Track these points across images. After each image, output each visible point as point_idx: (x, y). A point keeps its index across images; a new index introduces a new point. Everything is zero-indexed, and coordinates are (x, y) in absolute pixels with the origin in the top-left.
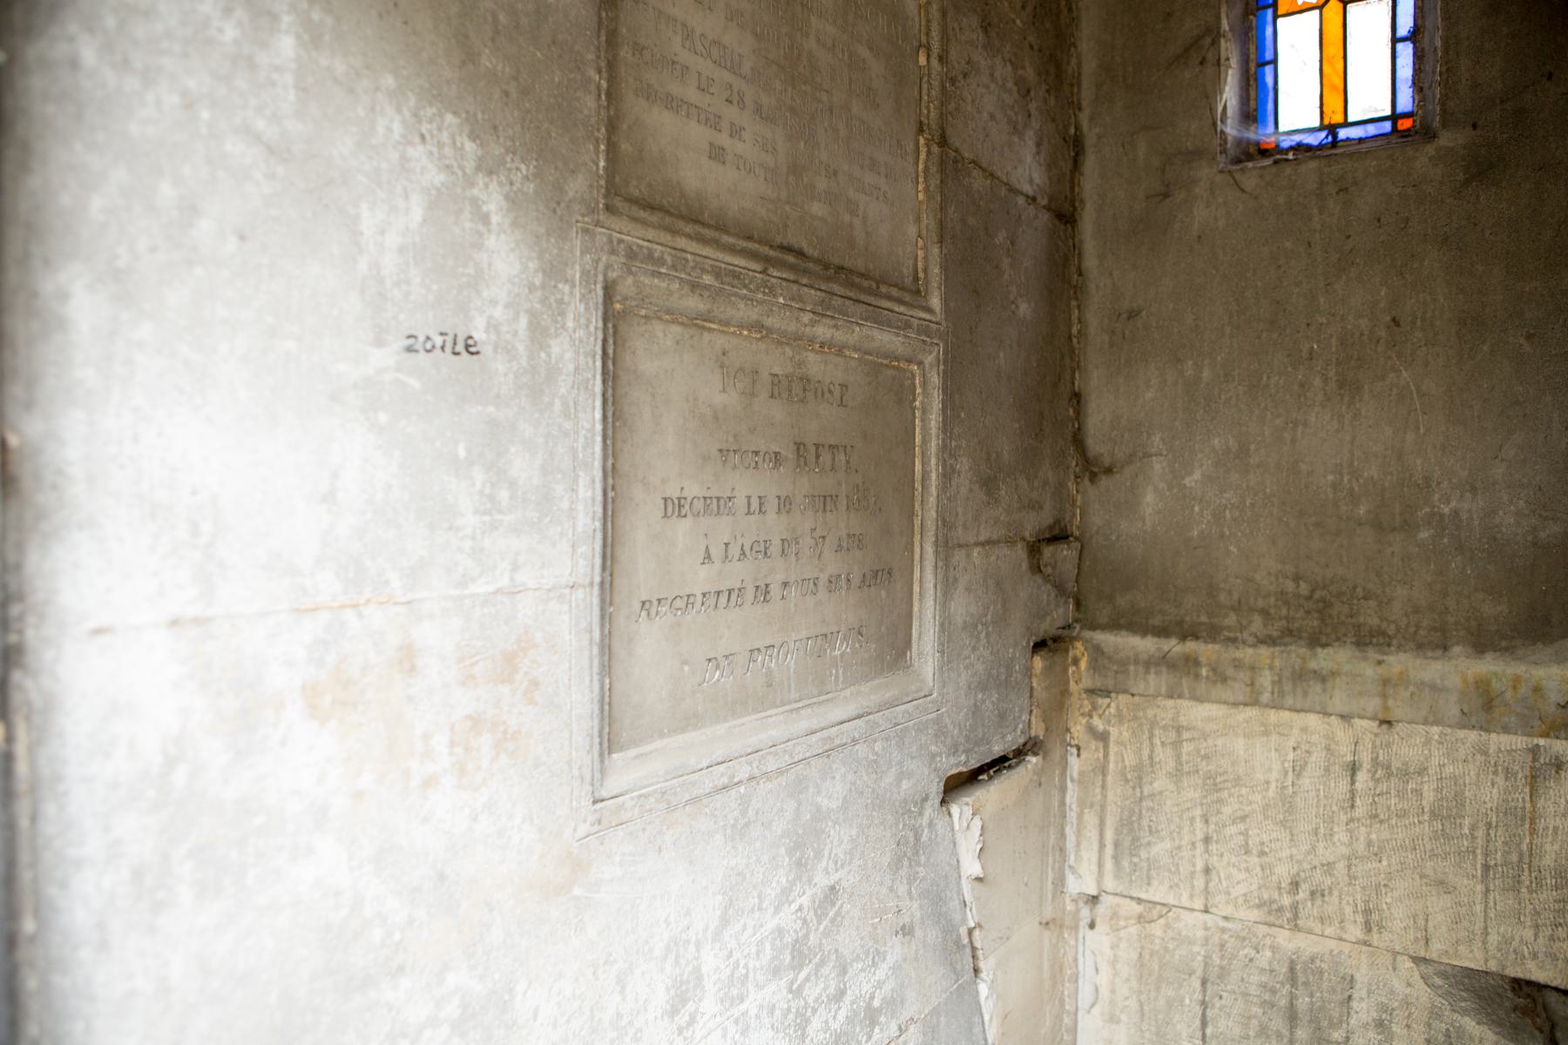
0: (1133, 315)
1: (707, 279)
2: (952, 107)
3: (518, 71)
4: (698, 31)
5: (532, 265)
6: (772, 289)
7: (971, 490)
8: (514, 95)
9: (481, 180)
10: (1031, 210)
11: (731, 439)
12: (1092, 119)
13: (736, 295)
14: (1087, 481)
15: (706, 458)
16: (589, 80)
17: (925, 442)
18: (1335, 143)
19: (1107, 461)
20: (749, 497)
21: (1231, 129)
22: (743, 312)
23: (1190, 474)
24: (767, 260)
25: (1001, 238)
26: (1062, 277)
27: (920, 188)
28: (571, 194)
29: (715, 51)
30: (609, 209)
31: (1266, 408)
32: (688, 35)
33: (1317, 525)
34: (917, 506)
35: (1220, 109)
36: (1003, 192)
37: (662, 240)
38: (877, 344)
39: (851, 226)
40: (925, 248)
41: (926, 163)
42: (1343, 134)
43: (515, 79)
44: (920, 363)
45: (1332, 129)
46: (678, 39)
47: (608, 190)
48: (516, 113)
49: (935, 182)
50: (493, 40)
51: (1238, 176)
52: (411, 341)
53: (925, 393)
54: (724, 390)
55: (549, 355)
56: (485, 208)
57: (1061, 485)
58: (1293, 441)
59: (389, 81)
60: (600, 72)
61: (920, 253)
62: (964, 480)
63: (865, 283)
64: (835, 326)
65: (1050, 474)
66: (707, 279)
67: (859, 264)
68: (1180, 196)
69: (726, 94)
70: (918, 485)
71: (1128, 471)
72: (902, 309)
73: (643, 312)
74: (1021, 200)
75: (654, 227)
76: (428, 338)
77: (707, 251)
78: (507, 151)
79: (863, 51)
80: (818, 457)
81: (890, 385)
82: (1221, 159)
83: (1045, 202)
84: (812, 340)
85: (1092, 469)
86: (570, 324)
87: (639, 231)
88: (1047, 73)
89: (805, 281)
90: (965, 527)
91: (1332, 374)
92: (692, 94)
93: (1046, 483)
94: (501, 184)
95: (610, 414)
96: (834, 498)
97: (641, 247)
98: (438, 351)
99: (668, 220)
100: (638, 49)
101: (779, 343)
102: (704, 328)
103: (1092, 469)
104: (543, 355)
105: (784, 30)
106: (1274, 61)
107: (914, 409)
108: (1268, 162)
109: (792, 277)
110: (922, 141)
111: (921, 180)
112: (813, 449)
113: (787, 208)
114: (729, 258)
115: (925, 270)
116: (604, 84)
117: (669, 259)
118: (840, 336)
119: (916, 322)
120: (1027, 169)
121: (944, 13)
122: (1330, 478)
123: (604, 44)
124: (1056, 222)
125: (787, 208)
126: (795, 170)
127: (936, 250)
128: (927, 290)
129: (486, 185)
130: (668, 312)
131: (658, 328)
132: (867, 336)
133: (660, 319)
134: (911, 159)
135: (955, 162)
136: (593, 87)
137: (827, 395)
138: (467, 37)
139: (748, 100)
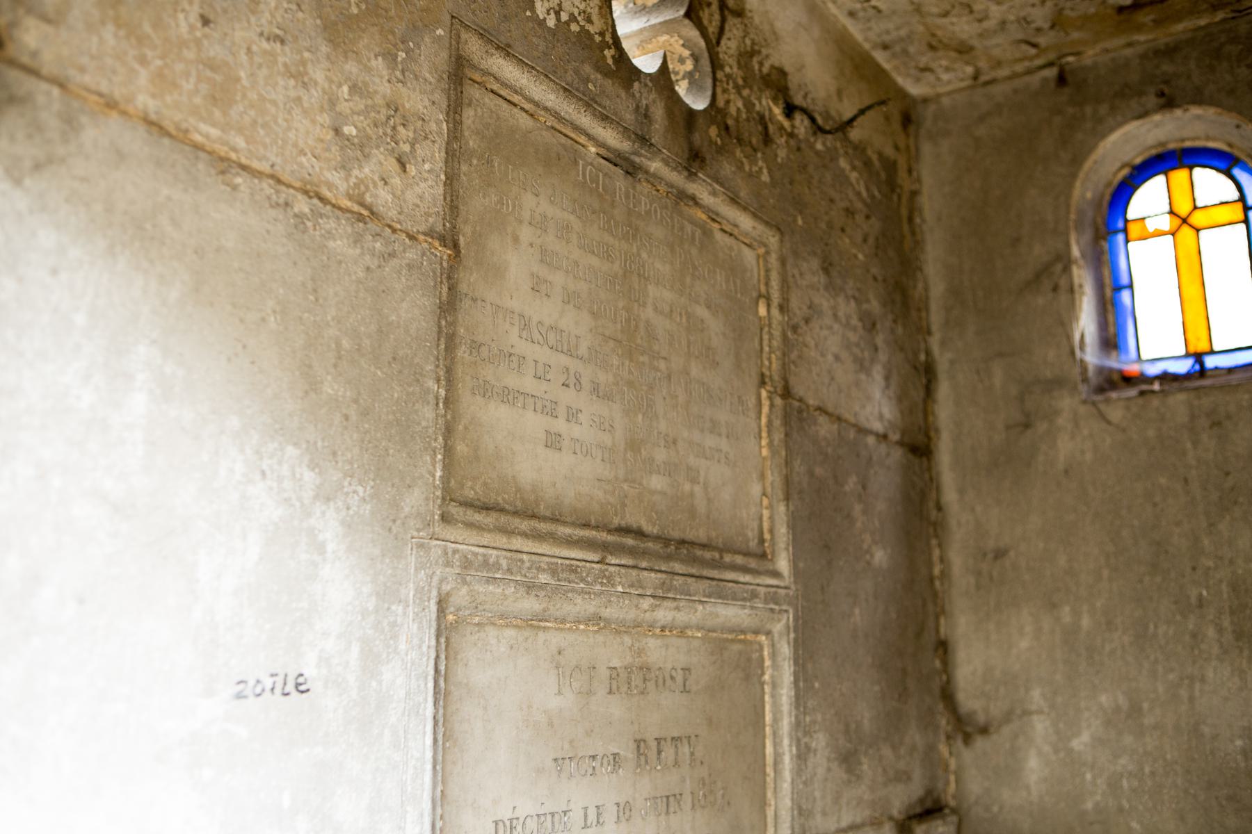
0: (1000, 554)
1: (544, 578)
2: (794, 356)
3: (359, 393)
4: (535, 320)
5: (366, 590)
6: (610, 578)
7: (829, 770)
8: (354, 418)
9: (318, 508)
10: (883, 448)
11: (567, 746)
12: (943, 343)
13: (573, 590)
14: (959, 742)
15: (540, 771)
16: (428, 391)
17: (776, 720)
18: (1203, 372)
19: (981, 719)
20: (586, 808)
21: (1091, 356)
22: (581, 606)
23: (1077, 734)
24: (605, 547)
25: (851, 484)
26: (920, 516)
27: (764, 442)
28: (407, 509)
29: (552, 337)
30: (445, 518)
31: (1156, 661)
32: (525, 325)
33: (1230, 798)
34: (770, 794)
35: (1077, 337)
36: (852, 434)
37: (497, 545)
38: (721, 620)
39: (692, 494)
40: (770, 507)
41: (769, 417)
42: (1210, 362)
43: (356, 401)
44: (768, 633)
45: (1198, 357)
46: (515, 331)
47: (444, 499)
48: (355, 436)
49: (778, 436)
50: (335, 366)
51: (1102, 407)
52: (241, 686)
53: (775, 666)
54: (559, 693)
55: (380, 683)
56: (321, 537)
57: (931, 749)
58: (1191, 699)
59: (234, 422)
60: (438, 381)
61: (766, 513)
62: (821, 761)
63: (708, 555)
64: (677, 608)
65: (917, 737)
66: (544, 578)
67: (701, 535)
68: (1042, 427)
69: (562, 379)
70: (770, 770)
71: (1006, 731)
72: (747, 578)
73: (476, 620)
74: (871, 440)
75: (489, 531)
76: (258, 682)
77: (544, 548)
78: (345, 475)
79: (701, 312)
80: (659, 752)
81: (738, 662)
82: (1083, 388)
83: (895, 437)
84: (651, 626)
85: (966, 729)
86: (403, 647)
87: (473, 537)
88: (893, 302)
89: (644, 564)
90: (824, 814)
91: (1226, 623)
92: (528, 383)
93: (913, 748)
94: (338, 510)
95: (440, 737)
96: (678, 797)
97: (476, 554)
98: (267, 694)
99: (504, 519)
100: (476, 346)
101: (618, 632)
102: (539, 627)
103: (966, 729)
104: (374, 684)
105: (621, 304)
106: (1130, 286)
107: (762, 684)
108: (1132, 392)
109: (630, 562)
110: (764, 394)
111: (764, 434)
112: (654, 744)
113: (625, 486)
114: (566, 553)
115: (771, 531)
116: (442, 392)
117: (504, 563)
118: (682, 617)
119: (762, 590)
120: (877, 406)
121: (783, 262)
122: (1239, 743)
123: (442, 353)
124: (910, 456)
125: (625, 486)
126: (634, 445)
127: (782, 508)
128: (773, 553)
129: (323, 513)
130: (502, 616)
131: (492, 632)
132: (711, 614)
133: (494, 624)
134: (753, 415)
135: (800, 411)
136: (431, 398)
137: (669, 682)
138: (310, 367)
139: (585, 382)
